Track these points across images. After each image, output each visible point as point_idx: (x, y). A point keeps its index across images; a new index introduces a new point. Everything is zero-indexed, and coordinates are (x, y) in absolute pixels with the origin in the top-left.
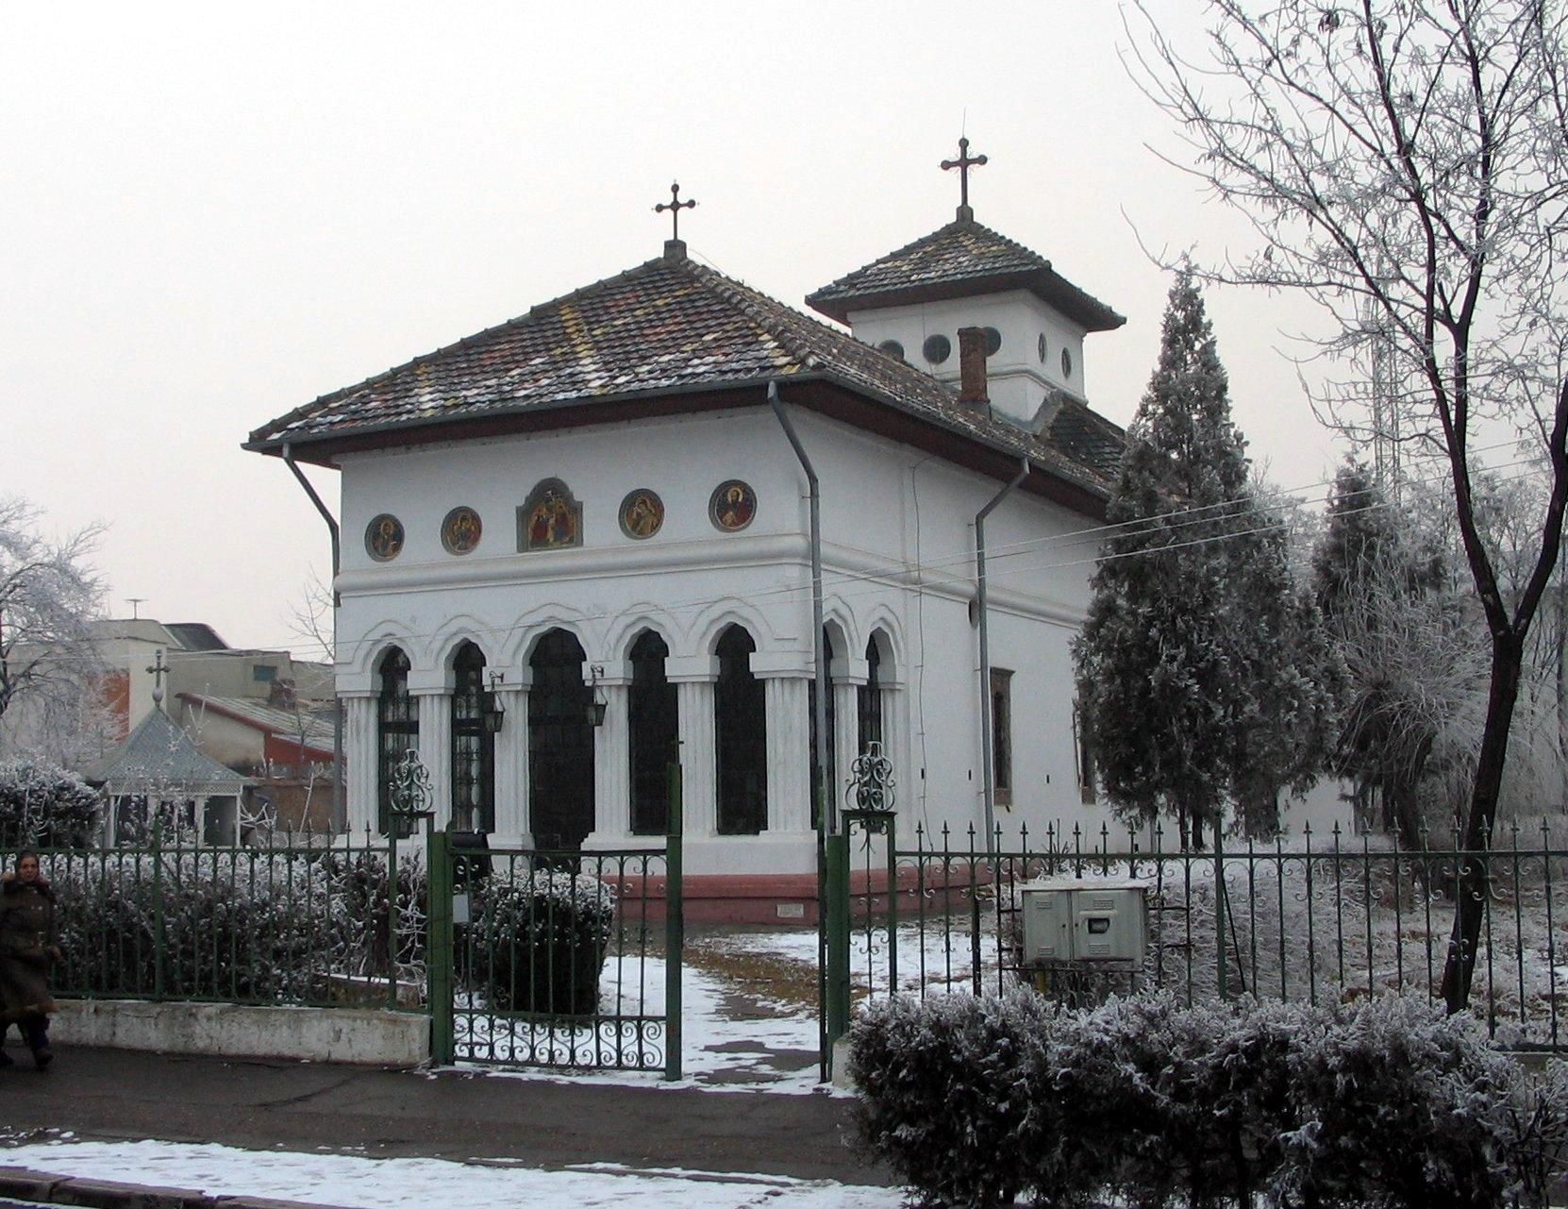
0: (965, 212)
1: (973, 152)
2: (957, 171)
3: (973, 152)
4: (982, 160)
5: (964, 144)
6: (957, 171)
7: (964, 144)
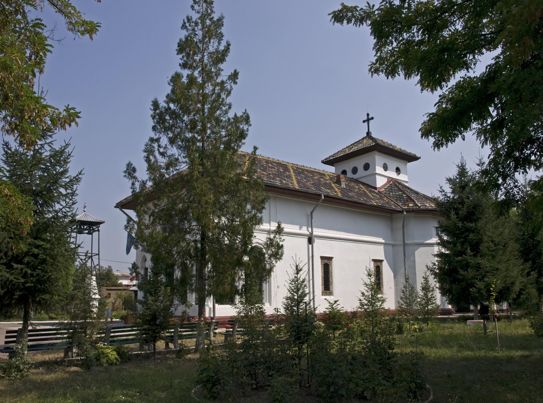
0: (368, 133)
1: (370, 117)
2: (366, 123)
3: (370, 117)
4: (372, 118)
5: (368, 115)
6: (366, 123)
7: (368, 115)
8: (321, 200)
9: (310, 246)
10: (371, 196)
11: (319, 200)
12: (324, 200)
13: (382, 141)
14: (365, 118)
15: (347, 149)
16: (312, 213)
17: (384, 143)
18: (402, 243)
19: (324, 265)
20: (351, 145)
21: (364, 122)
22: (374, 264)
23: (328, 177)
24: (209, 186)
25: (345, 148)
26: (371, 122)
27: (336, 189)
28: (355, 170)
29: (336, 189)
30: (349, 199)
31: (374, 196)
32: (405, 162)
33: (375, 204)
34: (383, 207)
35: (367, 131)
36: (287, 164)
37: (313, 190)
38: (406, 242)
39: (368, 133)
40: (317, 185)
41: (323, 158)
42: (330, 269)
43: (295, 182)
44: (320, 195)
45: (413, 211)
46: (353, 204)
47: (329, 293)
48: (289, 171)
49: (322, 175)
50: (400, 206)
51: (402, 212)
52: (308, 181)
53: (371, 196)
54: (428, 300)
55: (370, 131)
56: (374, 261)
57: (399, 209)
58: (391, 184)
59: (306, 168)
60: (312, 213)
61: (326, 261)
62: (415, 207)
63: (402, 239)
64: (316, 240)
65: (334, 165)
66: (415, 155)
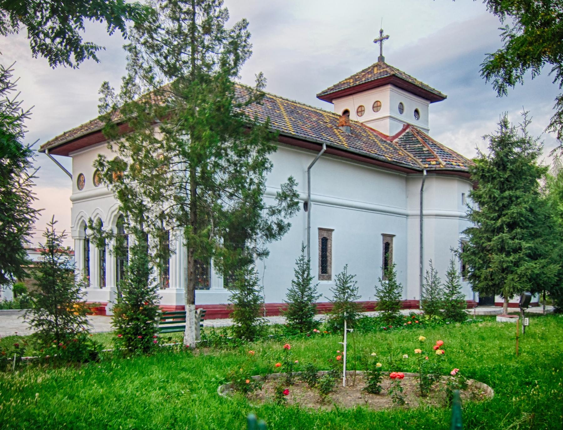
0: (381, 58)
1: (384, 34)
2: (378, 44)
3: (384, 34)
5: (381, 32)
6: (378, 44)
7: (381, 32)
8: (322, 151)
9: (307, 213)
10: (383, 149)
11: (320, 151)
12: (325, 152)
13: (398, 70)
14: (378, 36)
15: (352, 81)
16: (310, 168)
17: (401, 74)
18: (418, 212)
19: (322, 239)
20: (363, 71)
21: (376, 42)
22: (383, 240)
23: (327, 119)
24: (248, 99)
25: (350, 79)
26: (385, 42)
27: (341, 138)
28: (360, 111)
29: (341, 138)
30: (357, 151)
31: (387, 149)
32: (428, 102)
33: (390, 159)
34: (398, 164)
35: (379, 55)
36: (274, 98)
37: (312, 136)
38: (424, 212)
39: (381, 58)
40: (317, 129)
41: (319, 92)
42: (329, 246)
43: (289, 124)
44: (321, 145)
45: (435, 170)
46: (356, 156)
47: (327, 276)
48: (279, 109)
49: (319, 114)
50: (420, 164)
51: (422, 172)
52: (304, 123)
53: (383, 149)
54: (453, 289)
55: (383, 55)
56: (384, 235)
57: (416, 167)
58: (408, 133)
59: (298, 105)
60: (310, 168)
61: (325, 235)
62: (438, 166)
63: (420, 209)
64: (312, 205)
65: (333, 102)
66: (440, 93)
